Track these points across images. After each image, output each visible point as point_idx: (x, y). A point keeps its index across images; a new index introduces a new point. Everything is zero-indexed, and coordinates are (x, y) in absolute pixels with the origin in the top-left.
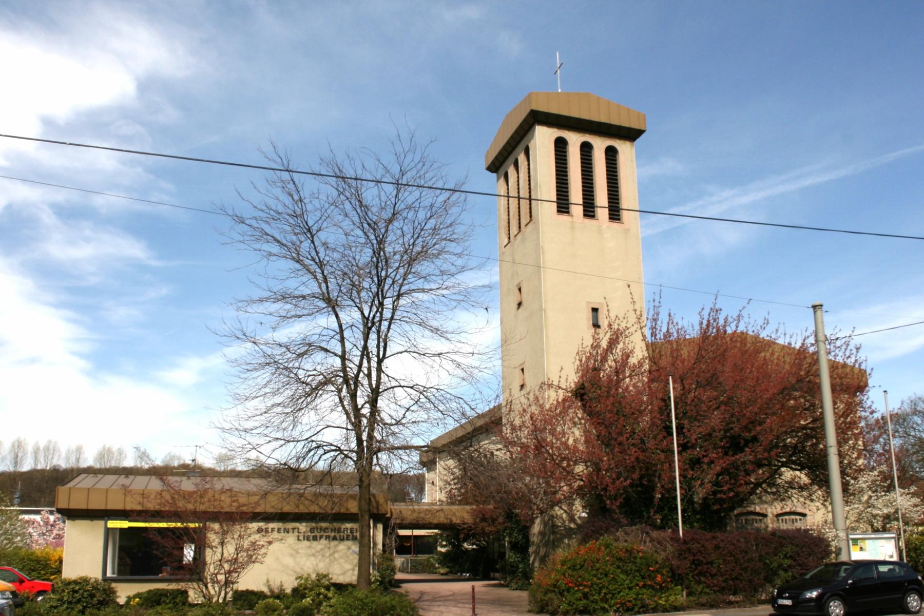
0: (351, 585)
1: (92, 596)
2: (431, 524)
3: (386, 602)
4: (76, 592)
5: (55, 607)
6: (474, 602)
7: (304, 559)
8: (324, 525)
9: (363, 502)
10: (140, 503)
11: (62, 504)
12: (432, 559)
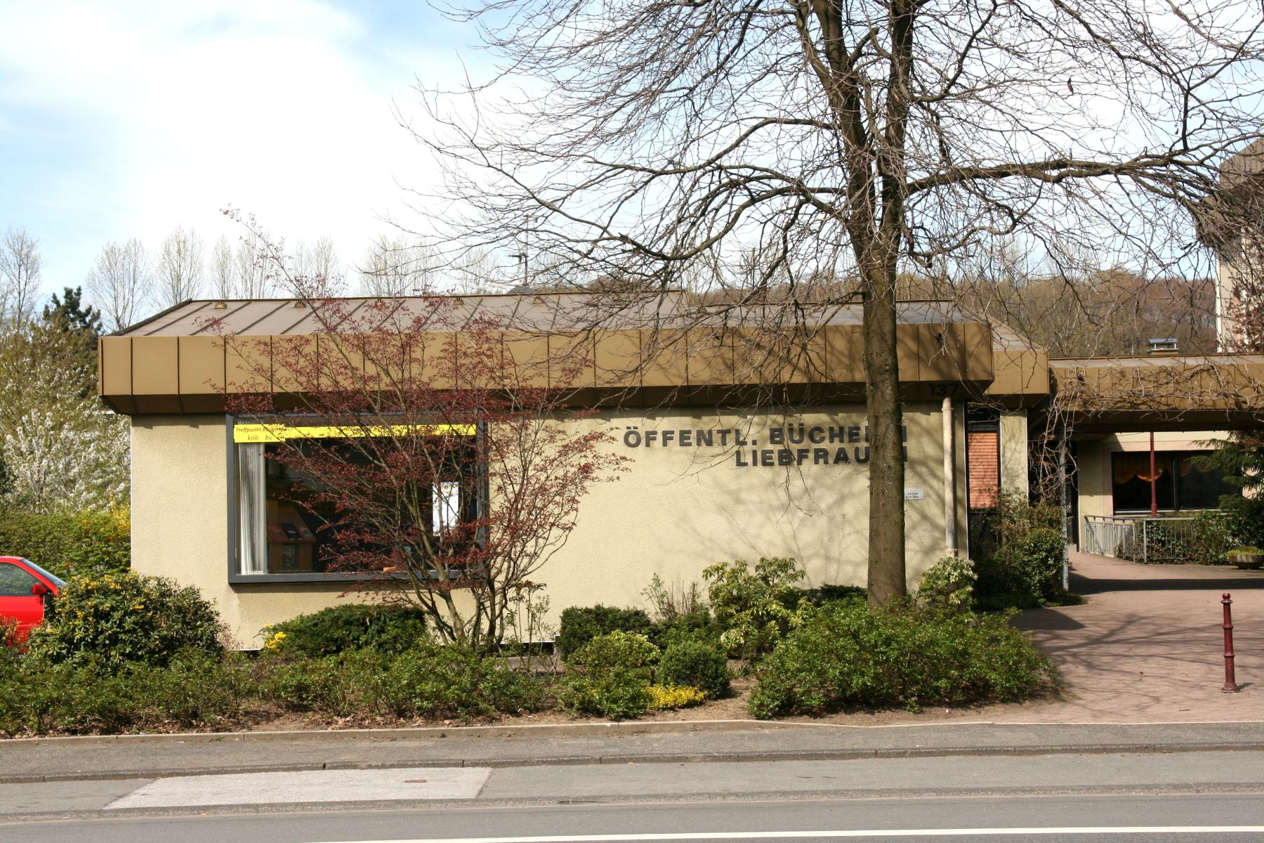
0: (858, 590)
1: (147, 626)
2: (1174, 412)
3: (933, 642)
4: (105, 616)
5: (58, 659)
6: (1229, 646)
7: (759, 518)
8: (810, 419)
9: (876, 346)
10: (259, 370)
11: (115, 385)
12: (1216, 517)
